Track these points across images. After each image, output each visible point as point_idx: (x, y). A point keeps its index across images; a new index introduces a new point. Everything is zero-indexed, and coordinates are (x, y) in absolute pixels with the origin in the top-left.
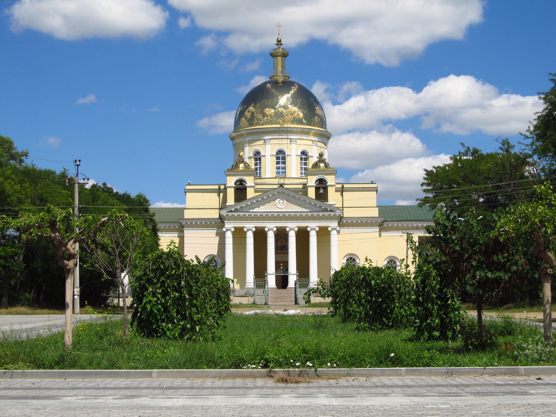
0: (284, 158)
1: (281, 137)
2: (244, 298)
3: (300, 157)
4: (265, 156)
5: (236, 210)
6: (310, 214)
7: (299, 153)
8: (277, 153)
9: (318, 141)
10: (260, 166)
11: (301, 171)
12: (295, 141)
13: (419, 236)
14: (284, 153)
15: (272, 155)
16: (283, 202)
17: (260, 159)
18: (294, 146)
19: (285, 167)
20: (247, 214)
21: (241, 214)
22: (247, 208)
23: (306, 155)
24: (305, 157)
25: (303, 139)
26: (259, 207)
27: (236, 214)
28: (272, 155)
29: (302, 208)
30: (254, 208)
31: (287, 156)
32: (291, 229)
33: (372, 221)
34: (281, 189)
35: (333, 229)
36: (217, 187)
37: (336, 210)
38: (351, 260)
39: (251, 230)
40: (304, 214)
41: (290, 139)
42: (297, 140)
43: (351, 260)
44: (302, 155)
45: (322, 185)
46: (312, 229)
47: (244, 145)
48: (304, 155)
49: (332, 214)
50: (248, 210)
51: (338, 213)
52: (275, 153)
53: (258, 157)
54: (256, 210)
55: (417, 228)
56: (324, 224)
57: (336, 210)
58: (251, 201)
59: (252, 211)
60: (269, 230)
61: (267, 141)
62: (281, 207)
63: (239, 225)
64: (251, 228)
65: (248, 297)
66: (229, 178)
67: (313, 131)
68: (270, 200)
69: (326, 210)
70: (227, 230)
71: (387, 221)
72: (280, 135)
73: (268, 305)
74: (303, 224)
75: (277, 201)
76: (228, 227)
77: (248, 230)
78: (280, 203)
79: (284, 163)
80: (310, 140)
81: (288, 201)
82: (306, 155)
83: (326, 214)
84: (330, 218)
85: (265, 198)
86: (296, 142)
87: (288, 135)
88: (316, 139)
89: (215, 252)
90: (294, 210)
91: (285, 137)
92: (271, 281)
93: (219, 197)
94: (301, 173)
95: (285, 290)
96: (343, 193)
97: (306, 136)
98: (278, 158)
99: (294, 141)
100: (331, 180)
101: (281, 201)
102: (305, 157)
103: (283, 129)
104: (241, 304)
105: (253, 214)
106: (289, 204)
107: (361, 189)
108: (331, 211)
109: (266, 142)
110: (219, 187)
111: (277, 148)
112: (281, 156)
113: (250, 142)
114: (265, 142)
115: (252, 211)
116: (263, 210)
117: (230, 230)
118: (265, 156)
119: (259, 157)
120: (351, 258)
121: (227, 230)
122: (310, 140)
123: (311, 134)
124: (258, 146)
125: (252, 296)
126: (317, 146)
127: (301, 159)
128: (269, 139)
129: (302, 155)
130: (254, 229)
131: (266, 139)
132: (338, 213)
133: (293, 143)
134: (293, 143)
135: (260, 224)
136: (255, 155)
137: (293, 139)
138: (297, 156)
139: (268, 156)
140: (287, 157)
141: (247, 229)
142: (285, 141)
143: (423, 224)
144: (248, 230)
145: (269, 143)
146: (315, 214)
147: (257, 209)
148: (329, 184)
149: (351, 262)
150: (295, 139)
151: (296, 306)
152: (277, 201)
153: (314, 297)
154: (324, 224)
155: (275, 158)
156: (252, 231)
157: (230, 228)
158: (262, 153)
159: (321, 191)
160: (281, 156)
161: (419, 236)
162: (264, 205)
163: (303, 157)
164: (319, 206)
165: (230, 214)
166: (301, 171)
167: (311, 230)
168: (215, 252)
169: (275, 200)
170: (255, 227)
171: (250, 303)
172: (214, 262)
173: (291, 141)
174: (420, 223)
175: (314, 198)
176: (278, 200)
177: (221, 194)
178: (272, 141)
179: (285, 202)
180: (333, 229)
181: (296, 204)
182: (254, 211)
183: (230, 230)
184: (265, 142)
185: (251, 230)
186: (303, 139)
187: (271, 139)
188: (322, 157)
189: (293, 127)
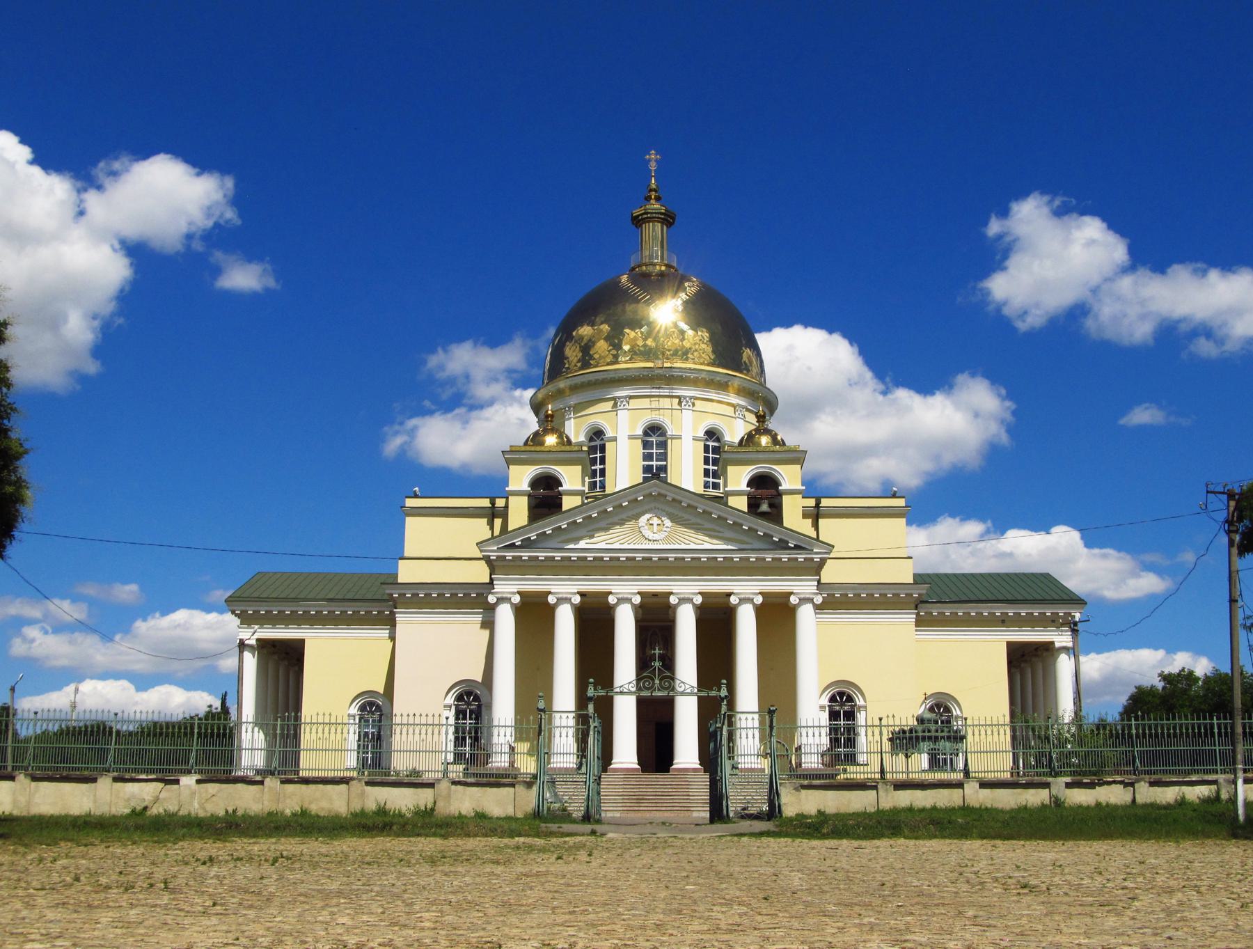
0: (663, 445)
1: (655, 392)
2: (495, 790)
3: (702, 443)
4: (614, 439)
5: (527, 544)
6: (736, 557)
7: (701, 434)
8: (646, 433)
9: (748, 410)
10: (602, 466)
11: (707, 467)
12: (690, 404)
13: (1009, 644)
14: (664, 434)
15: (632, 437)
16: (660, 522)
17: (603, 449)
18: (687, 415)
19: (666, 466)
20: (558, 555)
21: (542, 555)
22: (559, 540)
23: (718, 440)
24: (716, 444)
25: (711, 400)
26: (592, 537)
27: (525, 555)
28: (632, 437)
29: (715, 541)
30: (577, 540)
31: (672, 439)
32: (683, 600)
33: (898, 595)
34: (655, 485)
35: (804, 600)
36: (486, 503)
37: (813, 545)
38: (841, 698)
39: (568, 600)
40: (720, 557)
41: (679, 397)
42: (697, 402)
43: (841, 698)
44: (707, 440)
45: (765, 486)
46: (743, 601)
47: (564, 417)
48: (714, 441)
49: (801, 557)
50: (560, 546)
51: (817, 553)
52: (640, 432)
53: (598, 443)
54: (582, 544)
55: (1003, 621)
56: (776, 585)
57: (810, 544)
58: (570, 518)
59: (572, 546)
60: (621, 601)
61: (622, 402)
62: (656, 537)
63: (534, 585)
64: (569, 596)
65: (513, 785)
66: (514, 470)
67: (736, 383)
68: (624, 516)
69: (783, 545)
70: (501, 600)
71: (927, 602)
72: (653, 388)
73: (599, 822)
74: (717, 585)
75: (643, 519)
76: (504, 593)
77: (561, 601)
78: (652, 524)
79: (664, 456)
80: (728, 404)
81: (673, 519)
82: (718, 440)
83: (785, 556)
84: (795, 570)
85: (610, 509)
86: (694, 405)
87: (672, 389)
88: (743, 403)
89: (478, 676)
90: (693, 546)
91: (666, 392)
92: (626, 751)
93: (492, 528)
94: (706, 485)
95: (666, 775)
96: (820, 521)
97: (718, 394)
98: (646, 445)
99: (687, 402)
100: (789, 477)
101: (655, 521)
102: (716, 444)
103: (660, 371)
104: (481, 816)
105: (574, 556)
106: (679, 528)
107: (869, 511)
108: (797, 547)
109: (619, 404)
110: (493, 503)
111: (645, 419)
112: (655, 437)
113: (578, 408)
114: (615, 405)
115: (572, 546)
116: (603, 546)
117: (508, 600)
118: (614, 439)
119: (602, 442)
120: (841, 694)
121: (501, 600)
122: (728, 404)
123: (730, 389)
124: (599, 415)
125: (529, 785)
126: (744, 419)
127: (706, 449)
128: (625, 397)
129: (707, 440)
130: (577, 599)
131: (619, 398)
132: (817, 553)
133: (687, 407)
134: (687, 407)
135: (594, 585)
136: (591, 439)
137: (685, 397)
138: (695, 439)
139: (623, 442)
140: (669, 441)
141: (558, 599)
142: (666, 403)
143: (1033, 609)
144: (561, 601)
145: (627, 407)
146: (753, 557)
147: (588, 541)
148: (784, 486)
149: (842, 704)
150: (691, 398)
151: (720, 828)
152: (643, 520)
153: (796, 789)
154: (776, 585)
155: (639, 442)
156: (572, 604)
157: (509, 596)
158: (609, 433)
159: (765, 507)
160: (655, 437)
161: (1009, 644)
162: (606, 529)
163: (711, 444)
164: (764, 534)
165: (509, 555)
166: (707, 467)
167: (739, 604)
168: (478, 676)
169: (637, 517)
170: (582, 594)
171: (520, 815)
172: (473, 700)
173: (680, 403)
174: (1013, 609)
175: (746, 511)
176: (648, 516)
177: (498, 522)
178: (634, 403)
179: (668, 523)
180: (804, 600)
181: (698, 528)
182: (577, 546)
183: (508, 600)
184: (615, 405)
185: (568, 600)
186: (711, 400)
187: (631, 397)
188: (764, 422)
189: (685, 369)
